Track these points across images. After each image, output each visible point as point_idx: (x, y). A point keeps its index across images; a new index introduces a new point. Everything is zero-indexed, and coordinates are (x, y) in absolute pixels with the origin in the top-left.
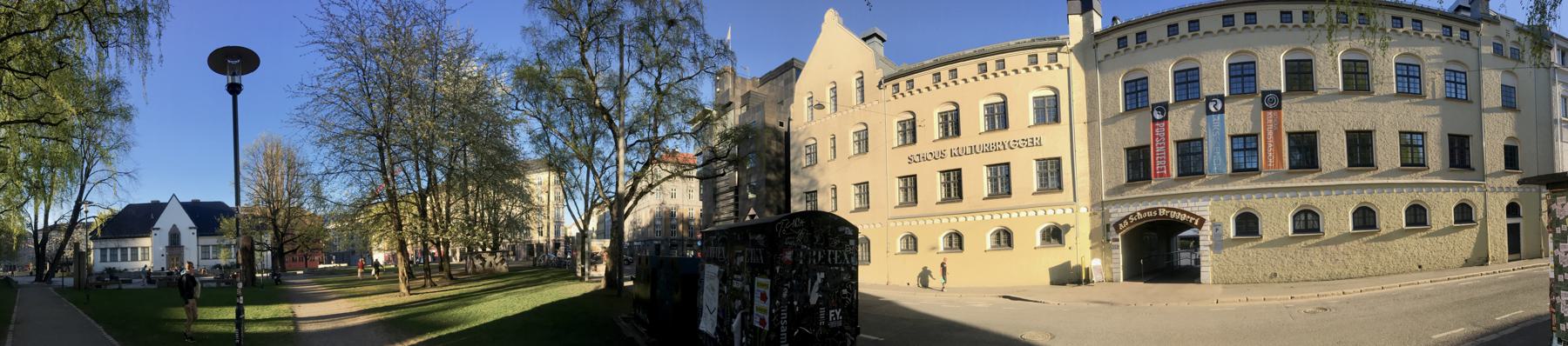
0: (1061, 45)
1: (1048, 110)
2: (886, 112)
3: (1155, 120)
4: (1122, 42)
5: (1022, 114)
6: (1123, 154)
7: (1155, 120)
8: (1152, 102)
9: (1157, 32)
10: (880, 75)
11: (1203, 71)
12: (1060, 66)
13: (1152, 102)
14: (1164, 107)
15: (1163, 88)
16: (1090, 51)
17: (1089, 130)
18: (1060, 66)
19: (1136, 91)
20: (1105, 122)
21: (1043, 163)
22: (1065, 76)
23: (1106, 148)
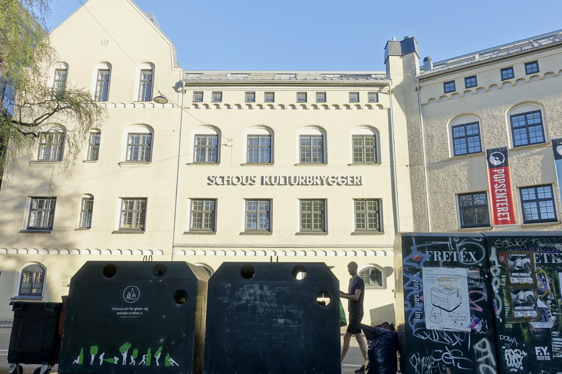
0: (382, 86)
1: (367, 150)
2: (178, 124)
3: (491, 166)
4: (449, 87)
5: (340, 151)
6: (455, 202)
7: (491, 166)
8: (485, 148)
9: (489, 76)
10: (178, 75)
11: (547, 114)
12: (381, 107)
13: (485, 148)
14: (502, 153)
15: (497, 130)
16: (410, 94)
17: (412, 174)
18: (381, 107)
19: (466, 137)
20: (431, 167)
21: (359, 203)
22: (386, 116)
23: (433, 193)
